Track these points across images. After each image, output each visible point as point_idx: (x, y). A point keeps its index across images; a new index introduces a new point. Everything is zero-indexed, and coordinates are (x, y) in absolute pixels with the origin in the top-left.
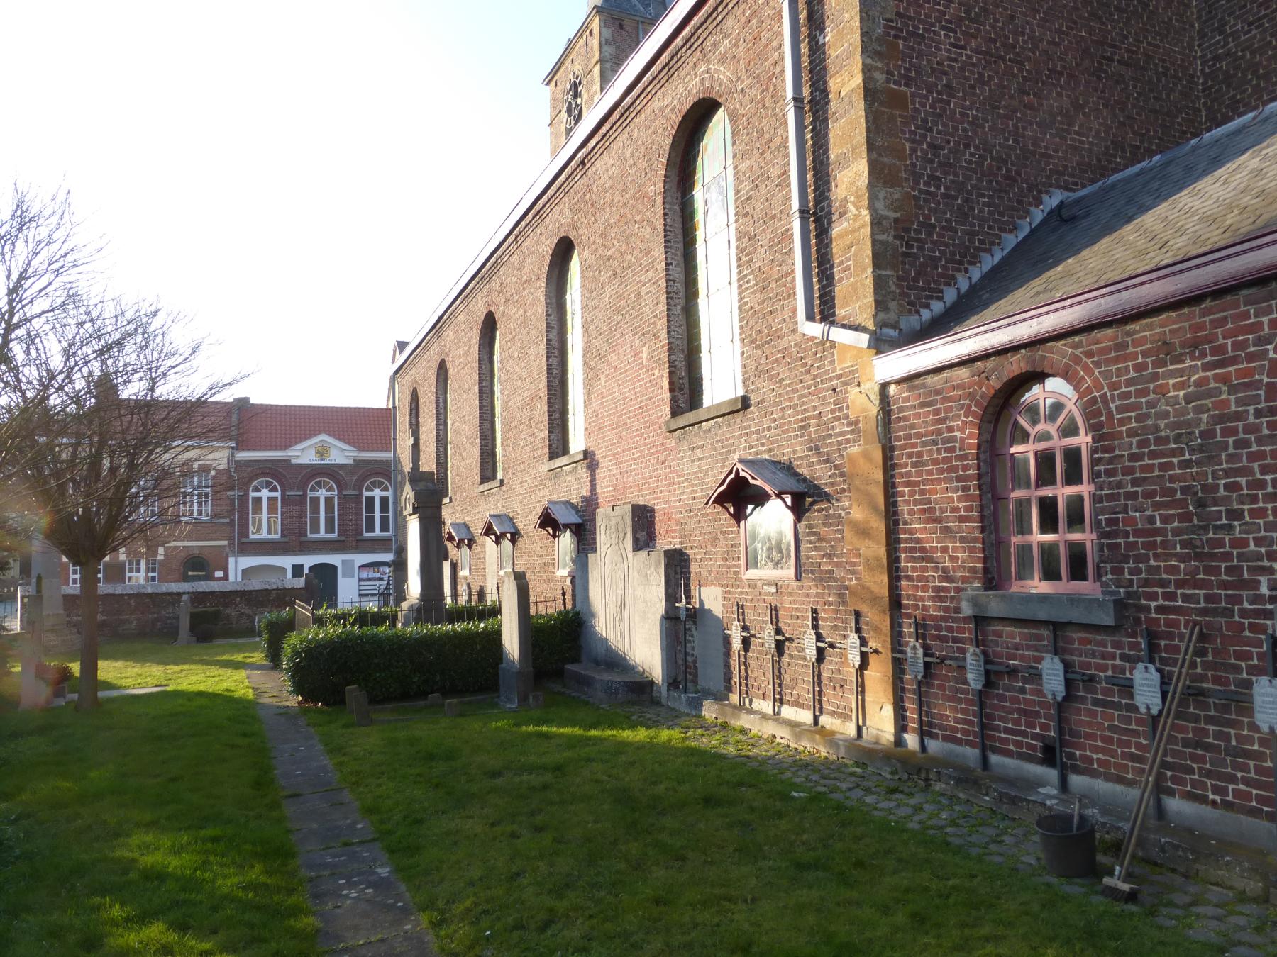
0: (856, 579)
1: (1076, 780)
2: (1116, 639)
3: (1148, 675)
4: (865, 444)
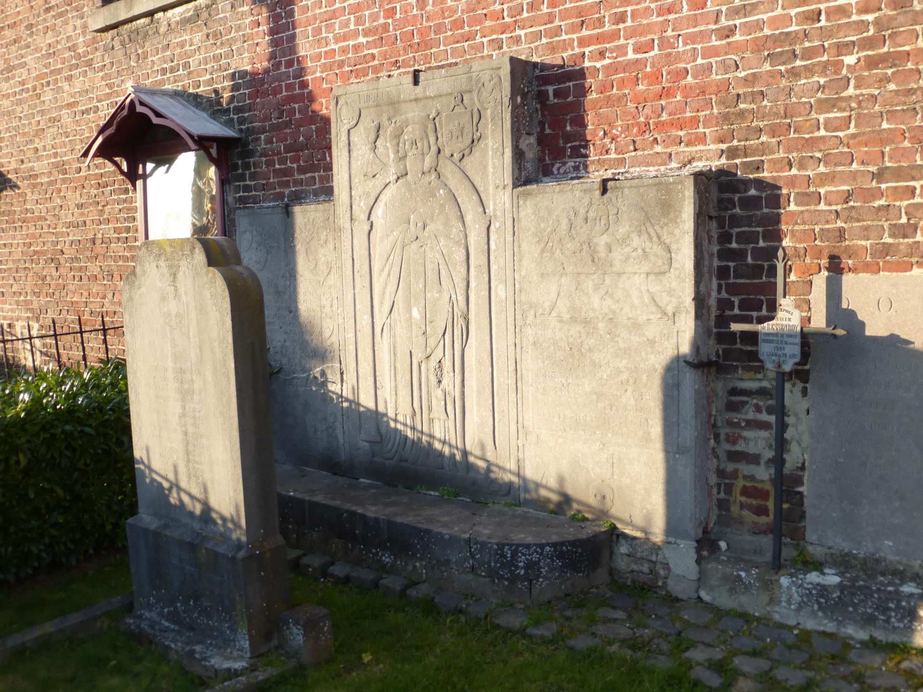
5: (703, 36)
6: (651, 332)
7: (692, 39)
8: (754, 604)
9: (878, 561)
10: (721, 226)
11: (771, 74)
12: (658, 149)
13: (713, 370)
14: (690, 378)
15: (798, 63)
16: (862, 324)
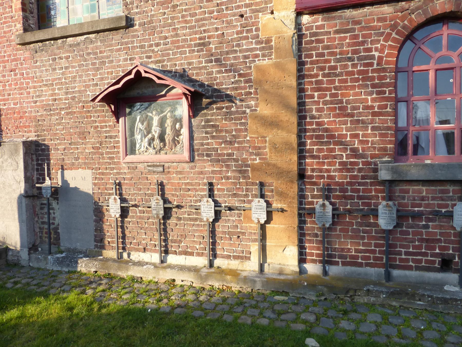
0: (260, 159)
3: (209, 204)
4: (276, 58)
5: (29, 102)
6: (14, 187)
7: (28, 103)
8: (42, 265)
9: (76, 249)
10: (36, 156)
11: (46, 115)
12: (20, 133)
13: (36, 198)
14: (24, 200)
15: (52, 112)
16: (69, 184)
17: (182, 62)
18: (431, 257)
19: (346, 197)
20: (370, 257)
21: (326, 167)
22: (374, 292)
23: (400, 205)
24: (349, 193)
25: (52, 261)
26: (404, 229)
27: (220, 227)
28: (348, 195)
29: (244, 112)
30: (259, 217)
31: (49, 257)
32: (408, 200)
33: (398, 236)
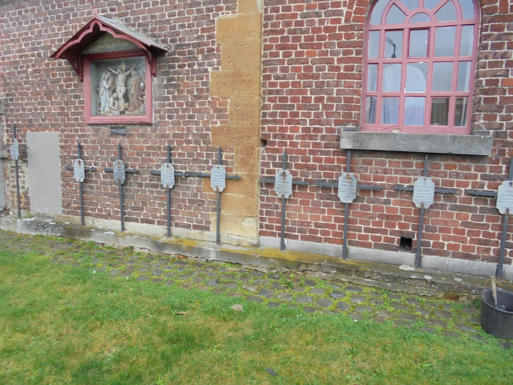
1: (175, 230)
2: (479, 164)
3: (169, 169)
8: (12, 228)
10: (6, 117)
13: (6, 160)
17: (145, 15)
18: (390, 235)
19: (307, 167)
20: (329, 232)
21: (288, 133)
22: (326, 268)
23: (363, 177)
24: (312, 163)
25: (21, 225)
26: (365, 203)
27: (180, 194)
28: (310, 164)
29: (206, 71)
30: (218, 185)
31: (18, 221)
32: (370, 172)
33: (359, 210)
